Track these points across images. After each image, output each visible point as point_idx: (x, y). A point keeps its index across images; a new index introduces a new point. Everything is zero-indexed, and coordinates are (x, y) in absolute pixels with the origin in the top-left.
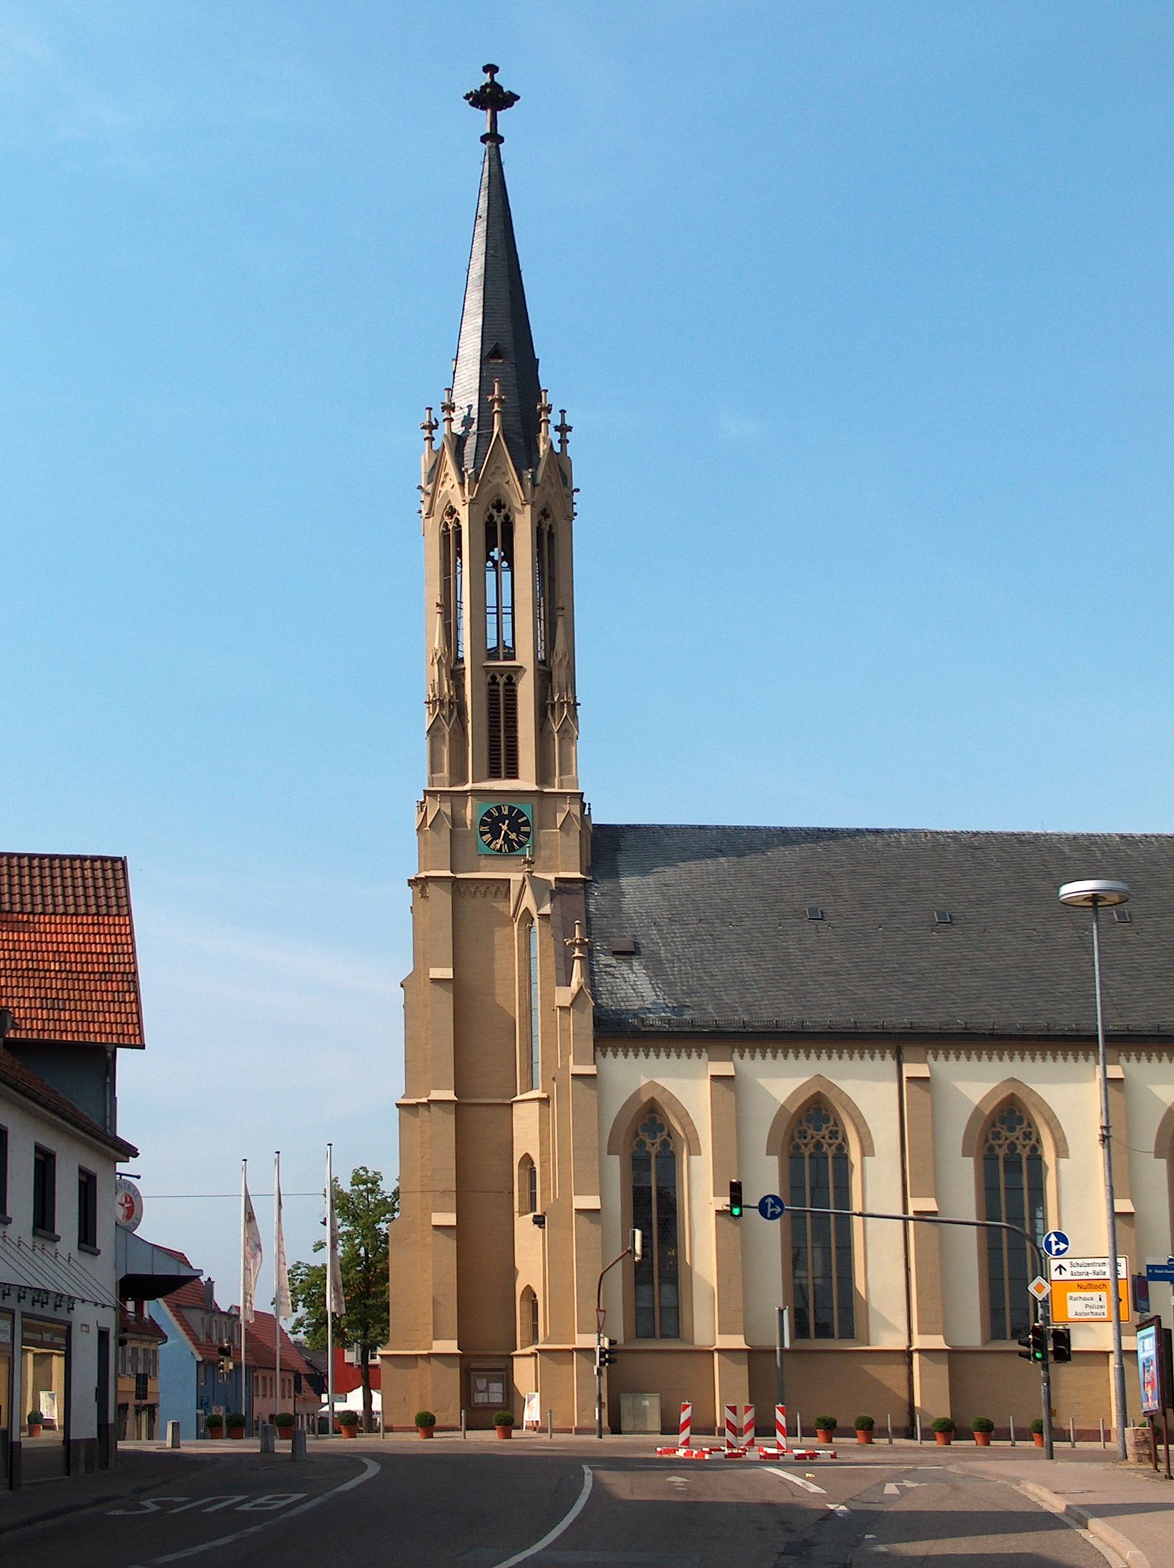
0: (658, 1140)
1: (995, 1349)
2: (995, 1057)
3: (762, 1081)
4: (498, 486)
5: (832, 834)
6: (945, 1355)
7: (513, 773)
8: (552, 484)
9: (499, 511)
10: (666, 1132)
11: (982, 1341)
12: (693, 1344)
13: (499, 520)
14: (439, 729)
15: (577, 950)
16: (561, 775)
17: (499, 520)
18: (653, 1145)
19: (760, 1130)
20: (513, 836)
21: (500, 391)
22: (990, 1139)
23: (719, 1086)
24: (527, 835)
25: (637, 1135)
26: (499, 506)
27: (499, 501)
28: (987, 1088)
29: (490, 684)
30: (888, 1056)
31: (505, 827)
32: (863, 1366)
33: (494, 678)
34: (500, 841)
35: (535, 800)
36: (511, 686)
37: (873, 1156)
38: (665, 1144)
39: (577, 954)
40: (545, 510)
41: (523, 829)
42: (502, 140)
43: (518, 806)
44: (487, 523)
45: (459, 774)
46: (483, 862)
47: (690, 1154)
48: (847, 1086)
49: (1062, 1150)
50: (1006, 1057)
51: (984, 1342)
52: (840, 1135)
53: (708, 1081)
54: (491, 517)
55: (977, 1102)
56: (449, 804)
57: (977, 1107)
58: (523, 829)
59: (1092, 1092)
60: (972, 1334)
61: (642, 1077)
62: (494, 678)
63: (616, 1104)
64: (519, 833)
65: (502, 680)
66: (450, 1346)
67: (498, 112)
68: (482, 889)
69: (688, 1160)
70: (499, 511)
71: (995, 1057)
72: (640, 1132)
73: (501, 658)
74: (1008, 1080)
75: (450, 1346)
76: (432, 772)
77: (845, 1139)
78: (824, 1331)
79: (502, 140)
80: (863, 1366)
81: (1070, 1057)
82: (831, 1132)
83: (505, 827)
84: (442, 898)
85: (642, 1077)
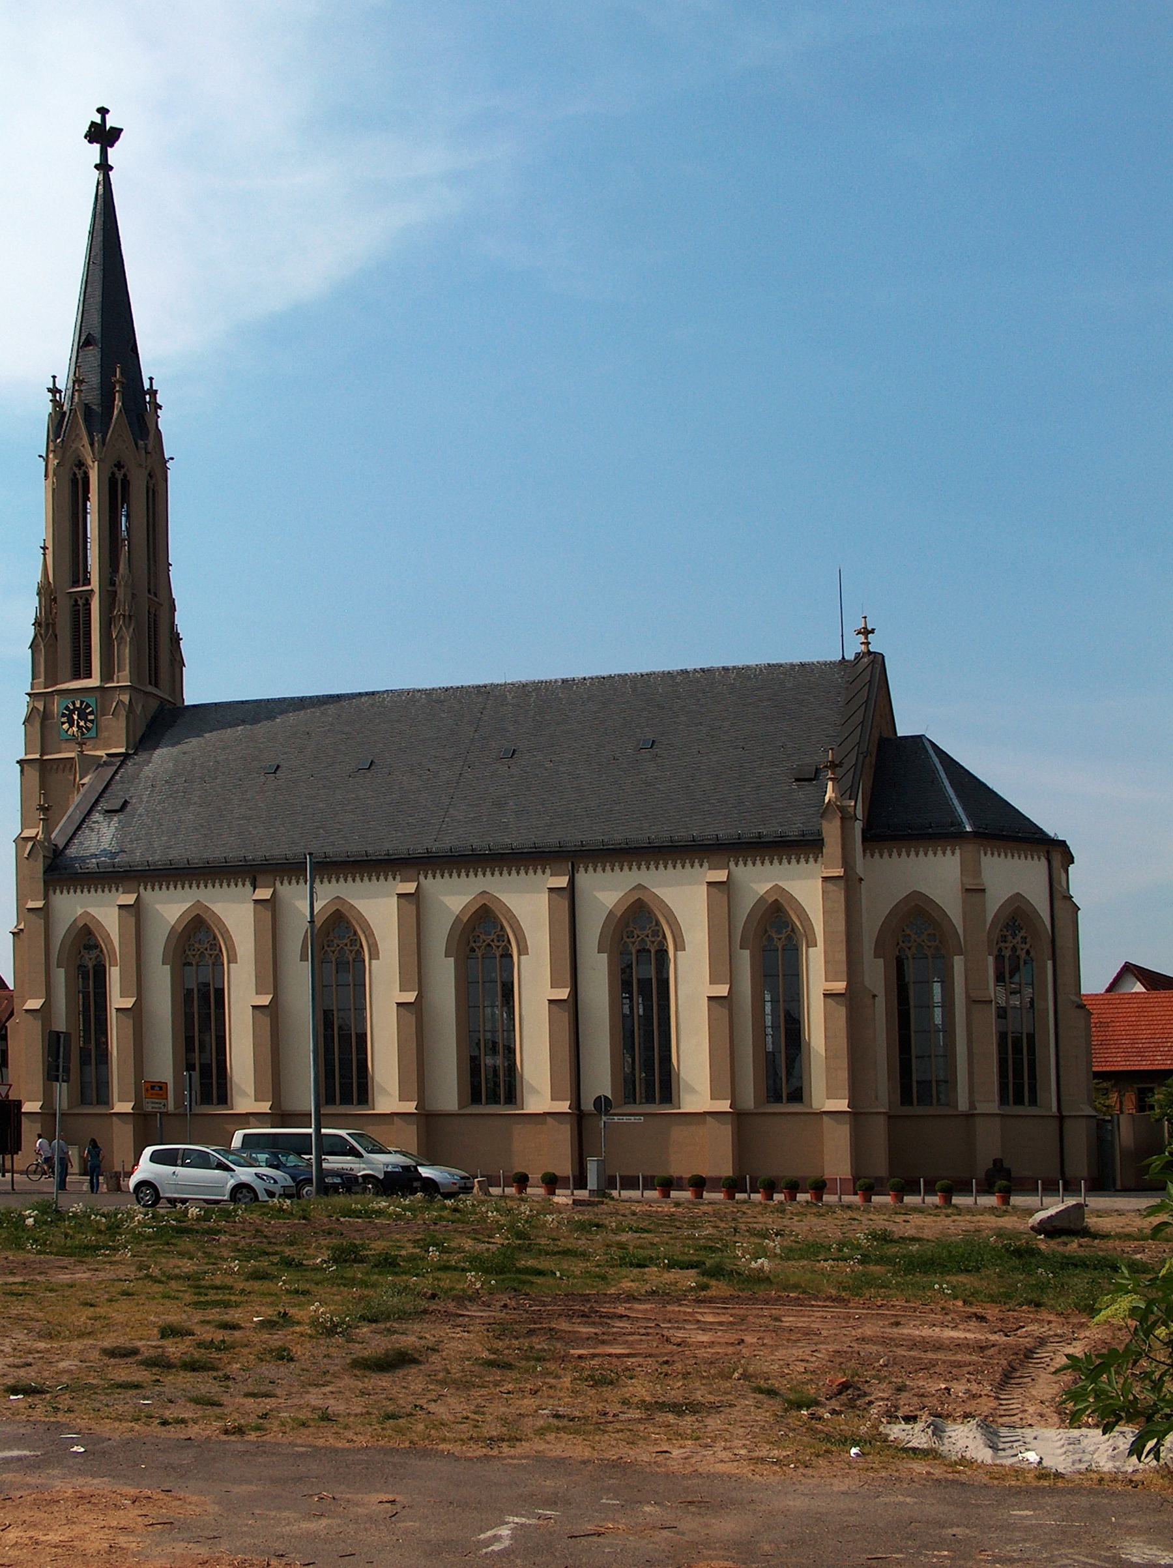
0: (783, 936)
1: (491, 1112)
2: (776, 861)
3: (158, 906)
4: (77, 449)
5: (338, 698)
6: (847, 1117)
7: (89, 676)
8: (124, 441)
9: (119, 470)
10: (789, 929)
11: (459, 1104)
12: (811, 1107)
13: (119, 476)
14: (38, 645)
15: (830, 772)
16: (118, 672)
17: (119, 476)
18: (780, 939)
19: (871, 927)
20: (82, 723)
21: (121, 373)
22: (625, 937)
23: (714, 890)
24: (92, 721)
25: (766, 931)
26: (119, 466)
27: (119, 462)
28: (466, 899)
29: (74, 606)
30: (248, 883)
31: (75, 717)
32: (226, 1126)
33: (76, 604)
34: (75, 729)
35: (98, 694)
36: (88, 604)
37: (378, 959)
38: (789, 938)
39: (830, 775)
40: (119, 462)
41: (90, 717)
42: (111, 168)
43: (87, 700)
44: (110, 478)
45: (52, 679)
46: (64, 745)
47: (808, 946)
48: (218, 908)
49: (523, 950)
50: (505, 872)
51: (461, 1107)
52: (661, 934)
53: (705, 887)
54: (113, 474)
55: (173, 923)
56: (42, 703)
57: (173, 927)
58: (90, 717)
59: (391, 905)
60: (749, 1102)
61: (79, 908)
62: (76, 601)
63: (746, 905)
64: (86, 721)
65: (80, 602)
66: (842, 1105)
67: (109, 149)
68: (61, 766)
69: (228, 967)
70: (119, 470)
71: (776, 861)
72: (82, 949)
73: (81, 583)
74: (633, 889)
75: (842, 1105)
76: (33, 679)
77: (664, 937)
78: (494, 1099)
79: (111, 168)
80: (226, 1126)
81: (514, 872)
82: (498, 936)
83: (75, 717)
84: (34, 774)
85: (79, 908)
